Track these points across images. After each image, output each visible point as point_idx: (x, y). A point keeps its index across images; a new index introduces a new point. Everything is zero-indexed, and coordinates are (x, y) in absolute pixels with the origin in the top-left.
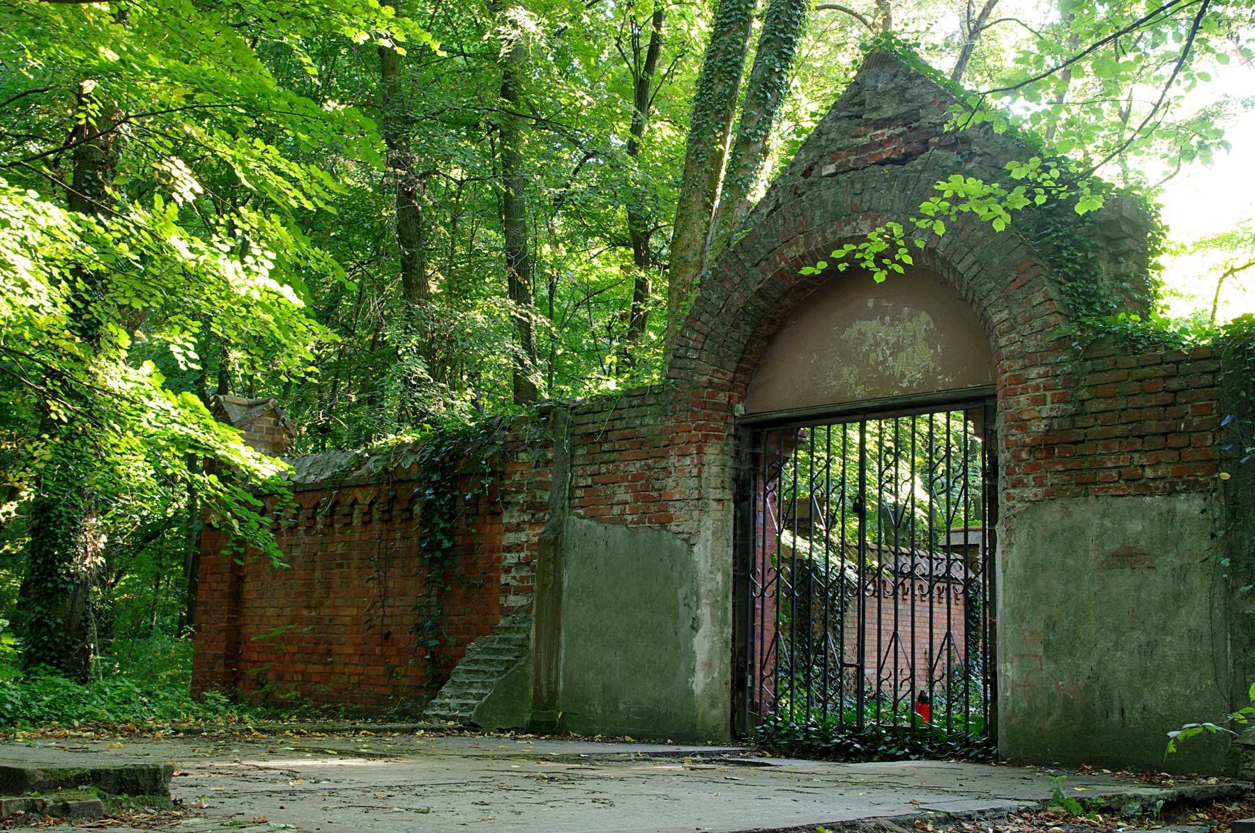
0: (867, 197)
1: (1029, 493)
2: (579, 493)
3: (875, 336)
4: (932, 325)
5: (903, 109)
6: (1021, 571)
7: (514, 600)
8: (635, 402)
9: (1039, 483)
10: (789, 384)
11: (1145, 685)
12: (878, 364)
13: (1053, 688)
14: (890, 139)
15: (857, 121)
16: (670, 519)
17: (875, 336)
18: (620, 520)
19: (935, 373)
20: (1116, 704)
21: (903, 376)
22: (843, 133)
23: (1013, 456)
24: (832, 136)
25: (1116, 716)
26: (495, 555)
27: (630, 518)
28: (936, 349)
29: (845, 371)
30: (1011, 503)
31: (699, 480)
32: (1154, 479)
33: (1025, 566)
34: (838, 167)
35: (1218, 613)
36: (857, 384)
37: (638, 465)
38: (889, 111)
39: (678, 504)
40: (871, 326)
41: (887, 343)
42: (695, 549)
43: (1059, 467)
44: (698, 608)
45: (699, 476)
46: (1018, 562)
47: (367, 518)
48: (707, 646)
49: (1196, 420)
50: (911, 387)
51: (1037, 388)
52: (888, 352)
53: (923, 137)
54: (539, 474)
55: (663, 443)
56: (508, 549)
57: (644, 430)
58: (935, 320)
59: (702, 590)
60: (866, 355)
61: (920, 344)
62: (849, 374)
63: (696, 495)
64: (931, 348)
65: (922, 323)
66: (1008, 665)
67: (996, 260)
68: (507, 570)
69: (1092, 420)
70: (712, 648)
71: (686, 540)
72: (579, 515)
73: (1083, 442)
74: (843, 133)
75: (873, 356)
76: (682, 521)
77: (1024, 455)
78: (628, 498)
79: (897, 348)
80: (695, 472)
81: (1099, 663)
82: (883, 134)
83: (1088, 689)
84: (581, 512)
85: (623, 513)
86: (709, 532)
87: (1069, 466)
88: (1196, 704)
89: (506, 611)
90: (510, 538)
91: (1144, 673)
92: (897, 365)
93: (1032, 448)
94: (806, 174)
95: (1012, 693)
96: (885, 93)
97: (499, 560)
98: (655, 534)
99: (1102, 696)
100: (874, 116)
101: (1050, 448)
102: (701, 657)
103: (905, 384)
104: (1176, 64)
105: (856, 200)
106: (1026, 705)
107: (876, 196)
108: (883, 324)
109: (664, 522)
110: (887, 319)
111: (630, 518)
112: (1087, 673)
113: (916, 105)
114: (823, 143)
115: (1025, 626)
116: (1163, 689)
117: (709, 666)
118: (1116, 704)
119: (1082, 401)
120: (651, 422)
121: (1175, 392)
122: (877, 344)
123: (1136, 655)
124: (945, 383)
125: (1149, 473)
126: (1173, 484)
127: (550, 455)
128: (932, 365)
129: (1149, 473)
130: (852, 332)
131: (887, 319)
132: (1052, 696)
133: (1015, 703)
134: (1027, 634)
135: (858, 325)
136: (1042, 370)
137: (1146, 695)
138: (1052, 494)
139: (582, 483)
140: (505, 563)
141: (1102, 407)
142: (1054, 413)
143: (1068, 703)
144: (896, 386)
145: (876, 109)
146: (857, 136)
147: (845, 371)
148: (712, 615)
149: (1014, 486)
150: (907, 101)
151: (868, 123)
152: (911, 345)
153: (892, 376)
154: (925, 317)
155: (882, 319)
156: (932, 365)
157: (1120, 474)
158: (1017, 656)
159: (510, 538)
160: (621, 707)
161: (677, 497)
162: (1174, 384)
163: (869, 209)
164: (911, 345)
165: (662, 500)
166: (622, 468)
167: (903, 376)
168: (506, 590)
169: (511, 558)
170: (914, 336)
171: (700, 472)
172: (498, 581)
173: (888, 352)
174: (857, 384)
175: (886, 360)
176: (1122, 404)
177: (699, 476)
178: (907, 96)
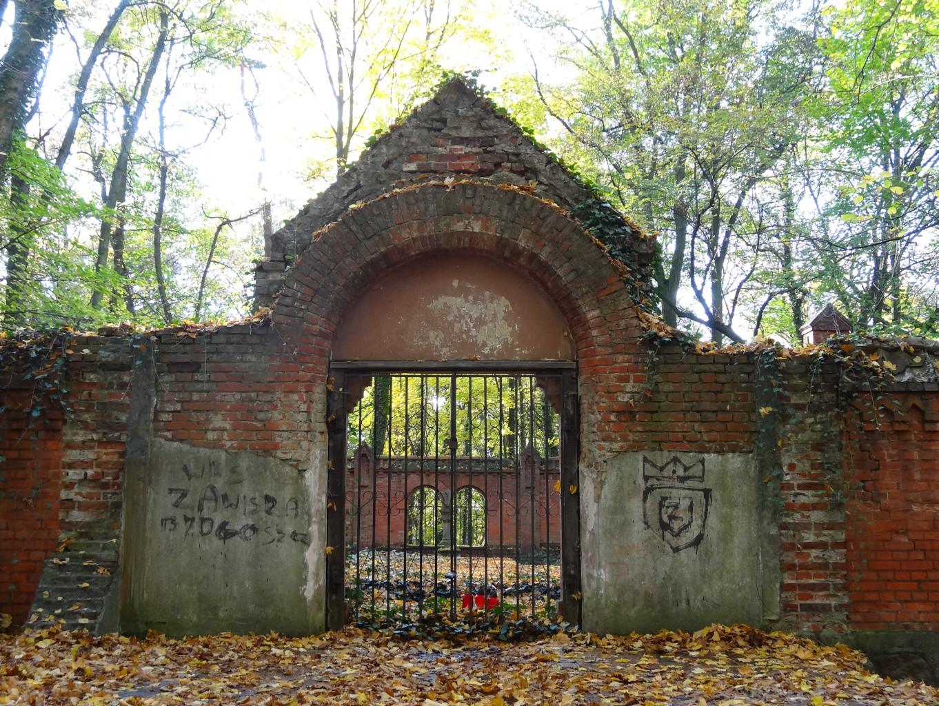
0: (478, 202)
1: (616, 446)
2: (164, 417)
3: (459, 310)
4: (510, 309)
5: (480, 134)
6: (612, 502)
7: (77, 516)
8: (234, 339)
9: (625, 439)
10: (373, 339)
11: (704, 583)
12: (462, 332)
13: (637, 587)
14: (467, 155)
15: (437, 133)
16: (276, 447)
17: (459, 310)
18: (216, 445)
19: (513, 346)
20: (684, 596)
21: (485, 344)
22: (424, 141)
23: (603, 418)
24: (413, 140)
25: (684, 605)
26: (52, 471)
27: (228, 444)
28: (514, 327)
29: (432, 334)
30: (603, 452)
31: (297, 415)
32: (709, 442)
33: (615, 499)
34: (419, 166)
35: (754, 534)
36: (442, 346)
37: (238, 396)
38: (466, 132)
39: (285, 435)
40: (456, 302)
41: (471, 317)
42: (307, 475)
43: (639, 429)
44: (309, 526)
45: (308, 412)
46: (609, 496)
47: (620, 518)
48: (315, 558)
49: (737, 405)
50: (492, 354)
51: (621, 370)
52: (471, 325)
53: (497, 160)
54: (111, 395)
55: (268, 380)
56: (71, 466)
57: (243, 365)
58: (512, 305)
59: (313, 510)
60: (451, 324)
61: (501, 322)
62: (435, 338)
63: (305, 427)
64: (509, 326)
65: (502, 305)
66: (602, 571)
67: (590, 272)
68: (70, 486)
69: (664, 397)
70: (319, 560)
71: (296, 467)
72: (167, 439)
73: (656, 412)
74: (424, 141)
75: (457, 326)
76: (288, 449)
77: (613, 418)
78: (227, 425)
79: (480, 322)
80: (304, 407)
81: (671, 568)
82: (461, 150)
83: (663, 586)
84: (169, 435)
85: (220, 439)
86: (317, 461)
87: (647, 429)
88: (739, 595)
89: (69, 526)
90: (73, 455)
91: (703, 575)
92: (481, 335)
93: (619, 413)
94: (387, 165)
95: (605, 591)
96: (465, 117)
97: (58, 476)
98: (261, 459)
99: (673, 591)
100: (454, 133)
101: (632, 414)
102: (311, 568)
103: (486, 351)
104: (353, 128)
105: (469, 203)
106: (616, 599)
107: (487, 203)
108: (467, 301)
109: (268, 450)
110: (471, 298)
111: (228, 444)
112: (662, 575)
113: (491, 133)
114: (404, 144)
115: (615, 542)
116: (717, 585)
117: (317, 575)
118: (684, 596)
119: (657, 383)
120: (254, 359)
121: (723, 384)
122: (461, 317)
123: (698, 563)
124: (521, 354)
125: (705, 437)
126: (722, 447)
127: (126, 379)
128: (510, 340)
129: (705, 437)
130: (438, 304)
131: (471, 298)
132: (636, 593)
133: (608, 597)
134: (616, 548)
135: (443, 300)
136: (626, 357)
137: (706, 589)
138: (635, 447)
139: (170, 407)
140: (67, 479)
141: (672, 389)
142: (635, 390)
143: (648, 596)
144: (479, 352)
145: (456, 128)
146: (437, 146)
147: (432, 334)
148: (319, 531)
149: (604, 440)
150: (483, 129)
151: (447, 137)
152: (492, 321)
153: (474, 344)
154: (504, 301)
155: (466, 297)
156: (510, 340)
157: (684, 437)
158: (610, 563)
159: (73, 455)
160: (221, 614)
161: (284, 428)
162: (722, 378)
163: (480, 213)
164: (492, 321)
165: (269, 428)
166: (218, 398)
167: (485, 344)
168: (69, 504)
169: (74, 475)
170: (495, 315)
171: (309, 407)
172: (57, 496)
173: (471, 325)
174: (442, 346)
175: (469, 330)
176: (687, 388)
177: (308, 412)
178: (484, 124)
